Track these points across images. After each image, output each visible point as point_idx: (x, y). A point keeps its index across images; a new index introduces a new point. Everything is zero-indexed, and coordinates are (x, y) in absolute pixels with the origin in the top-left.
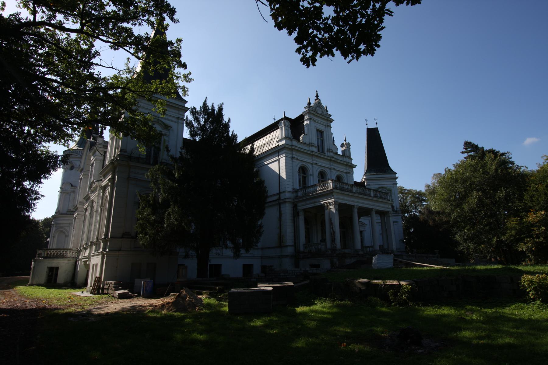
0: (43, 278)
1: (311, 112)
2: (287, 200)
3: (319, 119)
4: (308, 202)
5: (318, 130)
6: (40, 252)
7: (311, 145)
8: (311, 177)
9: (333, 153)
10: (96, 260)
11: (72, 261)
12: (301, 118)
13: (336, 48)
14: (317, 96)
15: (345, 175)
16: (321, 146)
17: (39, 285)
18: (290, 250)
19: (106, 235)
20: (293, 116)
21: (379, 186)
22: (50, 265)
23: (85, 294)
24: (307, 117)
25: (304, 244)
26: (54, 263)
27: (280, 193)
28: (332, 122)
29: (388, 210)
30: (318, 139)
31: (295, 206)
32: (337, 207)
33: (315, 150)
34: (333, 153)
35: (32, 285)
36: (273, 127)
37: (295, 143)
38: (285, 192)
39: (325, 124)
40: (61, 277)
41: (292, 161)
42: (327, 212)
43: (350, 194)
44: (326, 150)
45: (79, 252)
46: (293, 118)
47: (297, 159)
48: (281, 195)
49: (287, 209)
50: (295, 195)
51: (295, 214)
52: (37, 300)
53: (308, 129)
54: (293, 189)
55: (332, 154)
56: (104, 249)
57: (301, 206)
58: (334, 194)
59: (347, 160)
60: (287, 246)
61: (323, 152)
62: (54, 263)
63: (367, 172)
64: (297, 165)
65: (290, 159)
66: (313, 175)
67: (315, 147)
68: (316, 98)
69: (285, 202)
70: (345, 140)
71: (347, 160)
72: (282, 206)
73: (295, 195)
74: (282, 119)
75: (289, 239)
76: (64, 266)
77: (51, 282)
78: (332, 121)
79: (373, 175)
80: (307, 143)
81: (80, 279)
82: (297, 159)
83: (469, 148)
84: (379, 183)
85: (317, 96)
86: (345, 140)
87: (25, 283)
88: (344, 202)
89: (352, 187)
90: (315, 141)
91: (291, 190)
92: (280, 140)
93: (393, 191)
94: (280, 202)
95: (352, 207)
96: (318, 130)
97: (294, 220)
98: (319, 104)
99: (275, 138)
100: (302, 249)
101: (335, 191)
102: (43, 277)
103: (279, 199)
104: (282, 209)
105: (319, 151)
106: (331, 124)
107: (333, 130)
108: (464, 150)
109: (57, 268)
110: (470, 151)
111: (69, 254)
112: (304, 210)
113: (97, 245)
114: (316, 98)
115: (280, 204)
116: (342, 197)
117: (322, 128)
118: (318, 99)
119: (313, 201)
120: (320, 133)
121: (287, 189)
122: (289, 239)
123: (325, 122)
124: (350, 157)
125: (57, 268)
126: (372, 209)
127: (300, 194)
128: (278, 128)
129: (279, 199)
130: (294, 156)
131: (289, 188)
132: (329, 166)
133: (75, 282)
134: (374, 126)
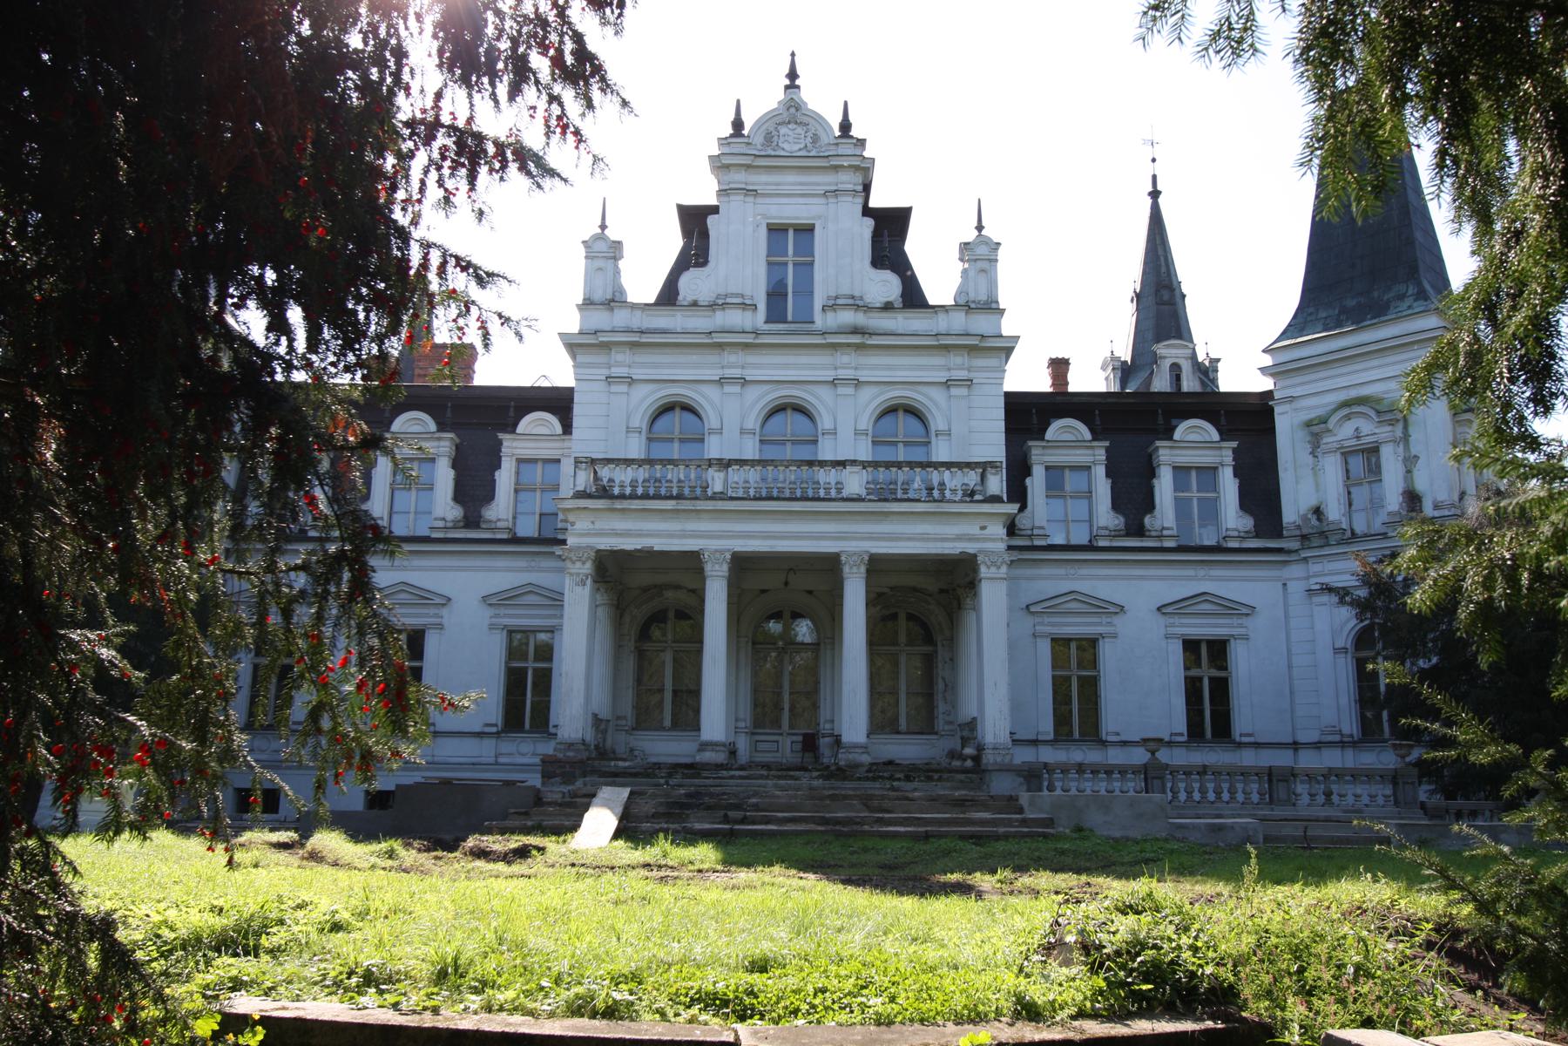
3: (791, 178)
14: (793, 75)
21: (1343, 396)
29: (970, 548)
34: (868, 309)
39: (821, 190)
43: (670, 504)
55: (848, 317)
59: (980, 324)
65: (602, 386)
70: (980, 228)
71: (980, 324)
79: (1318, 343)
85: (793, 75)
86: (980, 228)
90: (756, 285)
98: (793, 111)
116: (620, 524)
117: (792, 212)
124: (991, 307)
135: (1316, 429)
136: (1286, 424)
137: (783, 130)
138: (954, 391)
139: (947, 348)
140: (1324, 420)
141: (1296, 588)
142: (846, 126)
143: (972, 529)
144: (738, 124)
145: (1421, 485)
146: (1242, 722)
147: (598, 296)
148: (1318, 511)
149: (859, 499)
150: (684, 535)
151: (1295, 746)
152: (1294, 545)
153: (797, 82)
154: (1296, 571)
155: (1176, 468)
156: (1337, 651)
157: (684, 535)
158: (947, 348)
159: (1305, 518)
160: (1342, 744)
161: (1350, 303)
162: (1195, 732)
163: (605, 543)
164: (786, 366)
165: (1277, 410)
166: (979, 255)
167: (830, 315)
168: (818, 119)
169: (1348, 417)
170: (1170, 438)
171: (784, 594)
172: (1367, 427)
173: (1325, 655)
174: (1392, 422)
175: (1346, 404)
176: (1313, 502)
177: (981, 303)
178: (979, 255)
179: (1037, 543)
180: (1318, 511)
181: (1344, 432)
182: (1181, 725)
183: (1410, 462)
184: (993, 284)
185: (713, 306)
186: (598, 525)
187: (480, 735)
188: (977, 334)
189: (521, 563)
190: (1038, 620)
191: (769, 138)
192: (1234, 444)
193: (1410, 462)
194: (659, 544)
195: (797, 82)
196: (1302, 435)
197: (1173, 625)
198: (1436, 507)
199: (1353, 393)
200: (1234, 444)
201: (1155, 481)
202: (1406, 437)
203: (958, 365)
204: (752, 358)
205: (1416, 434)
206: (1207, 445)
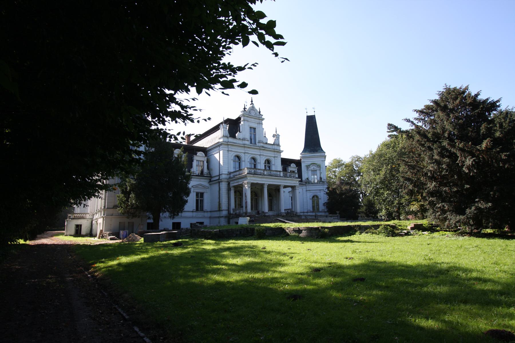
0: (73, 232)
3: (253, 119)
4: (235, 181)
5: (251, 128)
6: (70, 215)
7: (244, 139)
9: (263, 143)
10: (100, 221)
11: (90, 221)
12: (239, 119)
14: (252, 102)
15: (273, 158)
16: (253, 140)
17: (71, 235)
18: (225, 213)
19: (105, 207)
20: (234, 118)
22: (76, 224)
23: (96, 239)
24: (242, 119)
26: (79, 222)
31: (229, 184)
33: (248, 143)
34: (263, 143)
35: (66, 235)
36: (216, 128)
37: (231, 140)
38: (222, 174)
40: (84, 231)
42: (244, 188)
44: (257, 141)
45: (93, 215)
49: (224, 186)
50: (229, 176)
51: (229, 190)
52: (71, 241)
53: (243, 128)
55: (262, 144)
56: (104, 215)
59: (276, 147)
62: (79, 222)
63: (303, 152)
64: (232, 155)
71: (276, 147)
72: (220, 184)
73: (229, 176)
74: (222, 123)
75: (224, 206)
76: (85, 224)
77: (78, 233)
78: (263, 119)
80: (241, 138)
81: (94, 233)
83: (391, 128)
85: (252, 102)
87: (63, 234)
88: (255, 182)
90: (248, 137)
91: (227, 173)
92: (220, 138)
93: (321, 167)
95: (262, 185)
96: (251, 128)
100: (232, 212)
101: (248, 175)
102: (73, 231)
105: (251, 143)
107: (264, 126)
108: (389, 130)
109: (81, 225)
110: (393, 131)
111: (88, 216)
112: (234, 187)
113: (101, 212)
115: (219, 182)
116: (254, 179)
117: (254, 125)
119: (238, 181)
120: (253, 130)
122: (224, 206)
123: (258, 121)
124: (278, 145)
125: (81, 225)
127: (232, 175)
129: (219, 179)
131: (224, 171)
132: (259, 154)
133: (91, 234)
135: (308, 167)
136: (303, 166)
140: (309, 166)
141: (304, 190)
142: (260, 112)
144: (245, 109)
145: (322, 176)
146: (320, 210)
151: (304, 212)
154: (305, 187)
160: (311, 212)
162: (197, 209)
163: (252, 182)
166: (276, 136)
168: (256, 110)
171: (257, 190)
172: (315, 168)
173: (309, 200)
175: (312, 164)
177: (277, 144)
178: (276, 136)
180: (308, 179)
181: (312, 168)
183: (321, 173)
184: (279, 141)
187: (193, 212)
188: (276, 148)
189: (198, 180)
191: (250, 112)
193: (321, 173)
196: (306, 167)
203: (276, 154)
204: (248, 149)
205: (321, 169)
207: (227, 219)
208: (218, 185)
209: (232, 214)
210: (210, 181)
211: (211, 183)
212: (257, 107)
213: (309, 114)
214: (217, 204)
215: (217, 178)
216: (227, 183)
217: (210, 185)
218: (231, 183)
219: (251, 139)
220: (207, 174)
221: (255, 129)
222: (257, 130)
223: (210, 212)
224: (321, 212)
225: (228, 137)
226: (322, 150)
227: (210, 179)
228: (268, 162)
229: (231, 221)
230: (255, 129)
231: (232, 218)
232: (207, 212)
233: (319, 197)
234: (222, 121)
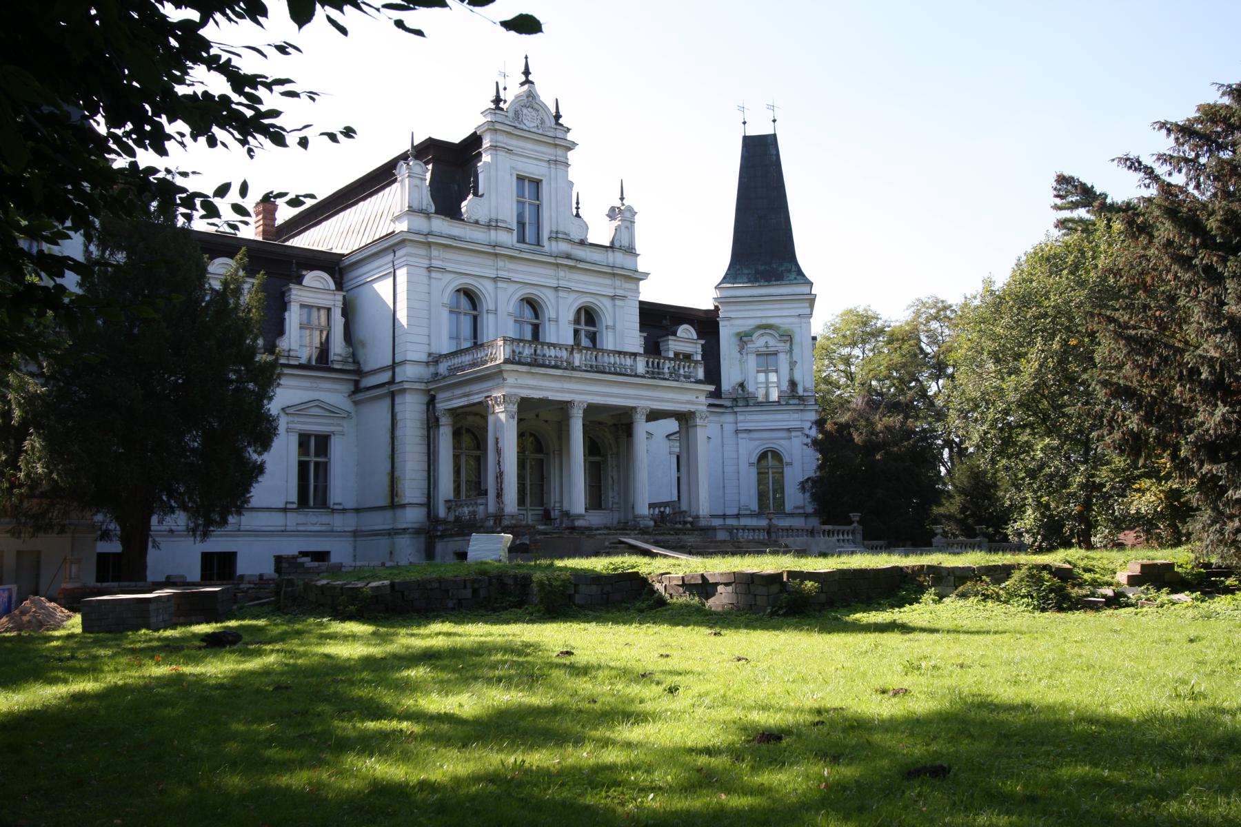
1: (498, 126)
2: (406, 386)
3: (530, 145)
4: (458, 392)
5: (521, 179)
8: (491, 317)
12: (474, 141)
13: (194, 162)
14: (527, 72)
16: (529, 227)
18: (413, 516)
20: (455, 135)
25: (447, 501)
27: (393, 367)
28: (570, 149)
29: (692, 408)
30: (520, 203)
31: (431, 402)
32: (515, 408)
33: (510, 239)
36: (380, 178)
37: (441, 225)
38: (403, 362)
39: (547, 157)
41: (430, 278)
42: (491, 419)
43: (559, 372)
44: (545, 234)
46: (457, 141)
47: (443, 270)
48: (397, 370)
49: (411, 409)
50: (432, 369)
51: (431, 424)
53: (489, 179)
54: (430, 355)
55: (564, 247)
57: (446, 402)
58: (505, 375)
59: (619, 258)
60: (404, 506)
61: (538, 243)
64: (445, 286)
65: (424, 272)
66: (496, 312)
67: (510, 230)
68: (523, 78)
69: (404, 391)
70: (622, 199)
71: (619, 258)
72: (398, 400)
73: (432, 369)
74: (404, 157)
75: (412, 489)
78: (571, 146)
79: (745, 290)
82: (443, 270)
83: (1068, 193)
84: (759, 314)
85: (527, 72)
86: (622, 199)
89: (572, 353)
94: (394, 388)
95: (563, 408)
96: (521, 179)
97: (428, 437)
98: (530, 99)
99: (384, 213)
100: (442, 512)
103: (392, 382)
104: (398, 408)
105: (522, 239)
106: (570, 154)
107: (573, 174)
108: (1059, 201)
110: (1074, 206)
112: (454, 412)
114: (523, 78)
115: (393, 395)
117: (534, 169)
118: (527, 82)
119: (467, 389)
120: (531, 186)
121: (411, 356)
122: (412, 489)
123: (549, 152)
124: (630, 251)
126: (634, 408)
127: (443, 368)
128: (395, 181)
129: (392, 382)
130: (435, 263)
134: (766, 130)
135: (743, 338)
137: (525, 111)
138: (500, 284)
139: (614, 275)
140: (749, 334)
141: (730, 428)
142: (558, 116)
143: (691, 397)
144: (498, 100)
145: (797, 378)
146: (788, 507)
147: (415, 206)
148: (742, 385)
149: (643, 377)
150: (563, 391)
151: (724, 516)
152: (728, 403)
153: (531, 78)
154: (729, 418)
155: (302, 306)
156: (751, 464)
157: (563, 391)
158: (614, 275)
159: (734, 388)
160: (751, 516)
161: (761, 268)
162: (303, 501)
164: (530, 273)
165: (721, 324)
167: (554, 243)
169: (762, 335)
170: (300, 283)
171: (541, 426)
172: (772, 342)
173: (744, 467)
174: (785, 342)
175: (760, 327)
176: (739, 380)
177: (623, 246)
178: (623, 215)
179: (292, 362)
180: (742, 385)
182: (294, 497)
183: (793, 364)
185: (488, 226)
186: (519, 381)
190: (291, 419)
191: (516, 112)
192: (703, 342)
193: (793, 364)
194: (552, 396)
195: (531, 78)
196: (735, 341)
197: (293, 422)
198: (805, 390)
199: (764, 322)
200: (703, 342)
201: (287, 314)
202: (791, 351)
203: (621, 287)
205: (796, 350)
206: (688, 340)
207: (422, 539)
208: (388, 401)
209: (445, 521)
210: (357, 389)
211: (359, 396)
212: (546, 97)
213: (753, 131)
214: (386, 481)
215: (385, 377)
216: (424, 399)
217: (356, 403)
218: (441, 396)
219: (521, 224)
220: (344, 362)
221: (537, 183)
222: (545, 187)
223: (357, 510)
224: (792, 515)
225: (427, 215)
226: (800, 273)
227: (356, 383)
228: (588, 316)
229: (439, 546)
230: (537, 183)
231: (442, 537)
232: (344, 511)
233: (786, 459)
234: (407, 146)
